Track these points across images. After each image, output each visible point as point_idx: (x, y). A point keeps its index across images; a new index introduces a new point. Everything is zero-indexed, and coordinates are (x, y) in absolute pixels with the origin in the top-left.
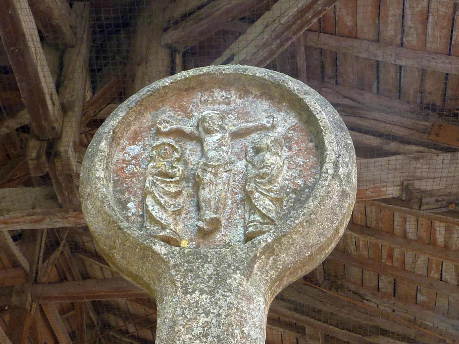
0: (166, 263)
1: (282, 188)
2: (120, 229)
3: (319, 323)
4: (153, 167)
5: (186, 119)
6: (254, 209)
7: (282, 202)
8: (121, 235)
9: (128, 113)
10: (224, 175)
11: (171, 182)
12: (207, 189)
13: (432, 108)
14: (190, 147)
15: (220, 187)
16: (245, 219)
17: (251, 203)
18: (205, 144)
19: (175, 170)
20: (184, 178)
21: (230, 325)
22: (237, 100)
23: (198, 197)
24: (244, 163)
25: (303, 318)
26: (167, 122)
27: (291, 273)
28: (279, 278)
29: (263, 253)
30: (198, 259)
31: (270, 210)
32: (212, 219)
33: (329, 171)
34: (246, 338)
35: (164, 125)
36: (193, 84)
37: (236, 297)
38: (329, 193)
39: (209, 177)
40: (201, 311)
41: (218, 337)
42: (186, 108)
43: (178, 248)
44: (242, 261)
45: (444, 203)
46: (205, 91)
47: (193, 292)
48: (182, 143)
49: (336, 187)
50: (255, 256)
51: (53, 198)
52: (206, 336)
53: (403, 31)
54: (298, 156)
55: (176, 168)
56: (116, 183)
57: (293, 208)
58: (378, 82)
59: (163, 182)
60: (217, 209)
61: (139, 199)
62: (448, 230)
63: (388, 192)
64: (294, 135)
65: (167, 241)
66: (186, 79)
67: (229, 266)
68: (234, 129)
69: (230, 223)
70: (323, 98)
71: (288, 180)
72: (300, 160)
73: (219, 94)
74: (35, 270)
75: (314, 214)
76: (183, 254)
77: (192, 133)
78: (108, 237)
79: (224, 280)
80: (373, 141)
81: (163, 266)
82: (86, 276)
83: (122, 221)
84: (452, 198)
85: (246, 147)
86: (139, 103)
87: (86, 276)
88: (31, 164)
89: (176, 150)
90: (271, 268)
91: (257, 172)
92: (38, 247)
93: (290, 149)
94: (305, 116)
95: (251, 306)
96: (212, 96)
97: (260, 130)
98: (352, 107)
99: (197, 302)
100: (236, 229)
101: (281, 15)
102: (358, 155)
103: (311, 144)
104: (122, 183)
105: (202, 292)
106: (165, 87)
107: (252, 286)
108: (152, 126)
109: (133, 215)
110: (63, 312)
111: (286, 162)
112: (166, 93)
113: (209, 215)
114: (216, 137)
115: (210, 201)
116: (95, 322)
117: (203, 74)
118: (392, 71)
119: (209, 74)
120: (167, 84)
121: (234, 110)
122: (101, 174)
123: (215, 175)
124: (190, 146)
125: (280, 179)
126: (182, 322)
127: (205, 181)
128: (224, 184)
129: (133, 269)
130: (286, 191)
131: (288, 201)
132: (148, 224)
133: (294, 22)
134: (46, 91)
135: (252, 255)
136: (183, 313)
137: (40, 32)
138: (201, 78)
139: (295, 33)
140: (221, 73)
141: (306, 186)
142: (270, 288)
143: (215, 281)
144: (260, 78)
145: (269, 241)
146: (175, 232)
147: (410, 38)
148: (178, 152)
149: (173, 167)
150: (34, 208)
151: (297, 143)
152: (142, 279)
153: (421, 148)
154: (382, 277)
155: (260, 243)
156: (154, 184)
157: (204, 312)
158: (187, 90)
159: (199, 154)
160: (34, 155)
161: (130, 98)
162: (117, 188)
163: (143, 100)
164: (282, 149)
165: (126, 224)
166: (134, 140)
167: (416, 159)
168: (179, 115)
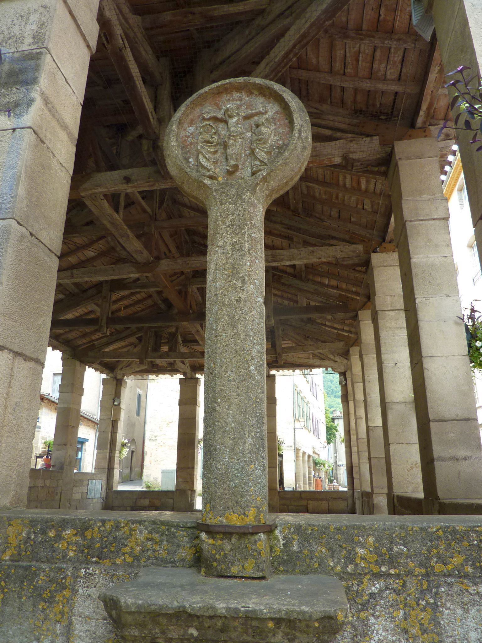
0: (210, 189)
1: (271, 146)
2: (186, 172)
3: (300, 235)
4: (202, 138)
5: (218, 110)
6: (256, 158)
7: (271, 154)
8: (187, 176)
9: (186, 108)
10: (240, 140)
11: (212, 146)
12: (231, 149)
13: (361, 111)
14: (221, 126)
15: (238, 147)
16: (251, 164)
17: (254, 155)
18: (229, 124)
19: (214, 139)
20: (218, 144)
21: (245, 219)
22: (246, 98)
23: (226, 154)
24: (250, 133)
25: (291, 232)
26: (208, 113)
27: (276, 192)
28: (270, 195)
29: (261, 181)
30: (227, 186)
31: (264, 158)
32: (234, 165)
33: (296, 135)
34: (253, 226)
35: (206, 114)
36: (221, 89)
37: (248, 206)
38: (296, 147)
39: (231, 142)
40: (230, 213)
41: (239, 226)
42: (218, 104)
43: (217, 181)
44: (250, 186)
46: (229, 93)
47: (225, 204)
48: (216, 124)
49: (300, 144)
50: (257, 183)
51: (159, 172)
52: (233, 226)
53: (345, 67)
54: (279, 128)
55: (214, 138)
56: (182, 148)
57: (277, 157)
59: (207, 146)
60: (237, 159)
61: (195, 157)
62: (368, 182)
63: (335, 161)
64: (278, 116)
65: (211, 177)
66: (217, 87)
67: (244, 189)
68: (244, 114)
69: (244, 167)
70: (293, 94)
71: (274, 142)
72: (280, 130)
73: (236, 95)
74: (154, 214)
75: (288, 159)
76: (219, 184)
77: (221, 118)
79: (241, 196)
80: (328, 132)
81: (209, 191)
82: (181, 216)
83: (187, 168)
85: (251, 125)
86: (192, 102)
87: (181, 216)
88: (145, 153)
89: (213, 128)
90: (266, 189)
91: (257, 138)
92: (155, 201)
93: (275, 124)
94: (283, 105)
95: (256, 210)
96: (232, 96)
97: (259, 114)
99: (227, 209)
100: (247, 170)
101: (276, 57)
102: (312, 125)
103: (287, 121)
104: (186, 148)
105: (230, 203)
106: (206, 92)
107: (256, 199)
108: (200, 116)
109: (193, 165)
110: (171, 236)
111: (273, 132)
112: (207, 96)
113: (232, 162)
114: (235, 119)
115: (232, 155)
116: (188, 240)
117: (226, 84)
118: (339, 91)
119: (230, 83)
120: (207, 90)
121: (244, 103)
122: (174, 143)
123: (235, 141)
124: (221, 125)
125: (269, 142)
126: (220, 219)
127: (230, 144)
128: (240, 145)
129: (195, 194)
130: (273, 148)
131: (274, 153)
132: (200, 170)
133: (283, 61)
134: (148, 110)
135: (255, 182)
136: (221, 215)
137: (143, 78)
138: (225, 86)
139: (283, 68)
140: (236, 82)
141: (284, 144)
142: (266, 200)
143: (236, 198)
144: (258, 84)
145: (264, 174)
146: (215, 173)
147: (348, 70)
148: (214, 129)
149: (212, 138)
150: (149, 178)
151: (279, 121)
153: (353, 135)
154: (333, 209)
155: (259, 176)
156: (202, 147)
157: (231, 214)
158: (218, 94)
159: (226, 129)
161: (187, 100)
162: (184, 151)
163: (194, 101)
164: (271, 124)
165: (189, 170)
166: (191, 124)
167: (351, 141)
168: (214, 108)
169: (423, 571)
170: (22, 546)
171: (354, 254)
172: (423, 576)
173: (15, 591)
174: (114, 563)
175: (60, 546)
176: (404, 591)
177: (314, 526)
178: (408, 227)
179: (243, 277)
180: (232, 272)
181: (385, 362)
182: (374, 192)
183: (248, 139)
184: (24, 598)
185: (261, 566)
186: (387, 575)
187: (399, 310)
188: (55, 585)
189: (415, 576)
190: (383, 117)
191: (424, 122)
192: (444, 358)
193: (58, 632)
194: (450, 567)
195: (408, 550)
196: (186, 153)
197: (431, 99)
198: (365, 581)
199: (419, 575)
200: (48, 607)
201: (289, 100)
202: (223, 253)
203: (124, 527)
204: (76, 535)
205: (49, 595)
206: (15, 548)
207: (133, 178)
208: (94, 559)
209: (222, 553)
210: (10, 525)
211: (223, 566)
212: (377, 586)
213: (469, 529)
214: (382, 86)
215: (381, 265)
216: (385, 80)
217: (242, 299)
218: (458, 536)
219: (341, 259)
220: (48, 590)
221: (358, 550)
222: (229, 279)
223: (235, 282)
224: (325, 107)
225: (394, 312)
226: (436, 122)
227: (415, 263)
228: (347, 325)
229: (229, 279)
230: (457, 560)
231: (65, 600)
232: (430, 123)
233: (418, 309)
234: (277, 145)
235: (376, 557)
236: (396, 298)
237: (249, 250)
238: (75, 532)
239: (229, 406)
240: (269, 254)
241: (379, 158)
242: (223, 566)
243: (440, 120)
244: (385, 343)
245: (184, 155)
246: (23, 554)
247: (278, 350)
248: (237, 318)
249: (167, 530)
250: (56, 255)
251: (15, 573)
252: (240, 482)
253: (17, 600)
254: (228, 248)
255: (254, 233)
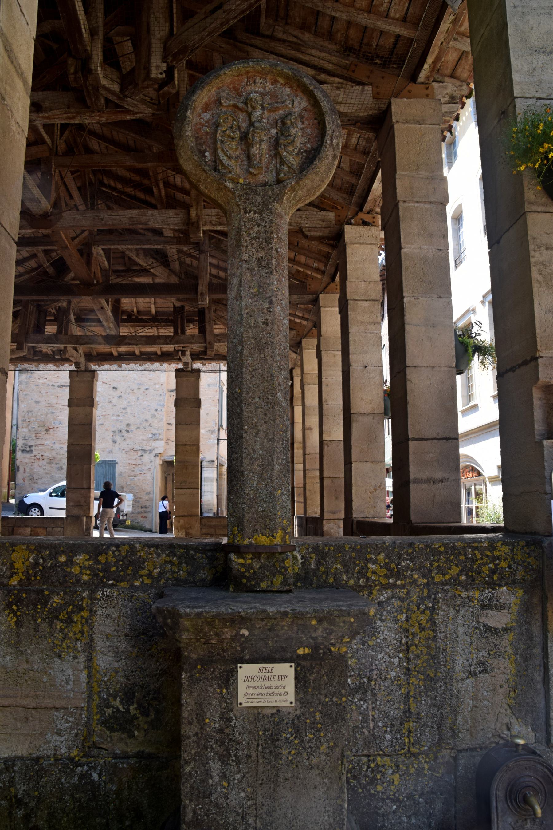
24: (275, 130)
41: (265, 239)
45: (354, 122)
58: (316, 27)
67: (270, 197)
78: (196, 175)
84: (359, 119)
90: (293, 199)
93: (303, 123)
94: (312, 101)
98: (296, 44)
103: (316, 121)
105: (255, 213)
150: (69, 107)
151: (307, 120)
152: (217, 201)
153: (341, 81)
160: (72, 71)
167: (338, 88)
169: (425, 581)
170: (31, 572)
171: (324, 224)
172: (424, 585)
173: (29, 614)
174: (132, 586)
175: (73, 570)
176: (407, 599)
177: (331, 546)
178: (401, 209)
179: (270, 297)
180: (259, 292)
181: (353, 364)
182: (355, 149)
183: (273, 137)
184: (40, 620)
185: (289, 581)
186: (394, 586)
187: (374, 300)
188: (71, 607)
189: (419, 586)
190: (378, 61)
191: (428, 78)
192: (429, 369)
193: (80, 649)
194: (447, 577)
195: (414, 565)
196: (201, 145)
197: (439, 52)
198: (375, 592)
199: (420, 585)
200: (66, 627)
201: (321, 99)
202: (248, 269)
203: (139, 551)
204: (88, 560)
205: (66, 616)
206: (23, 573)
207: (47, 104)
208: (110, 582)
209: (252, 571)
210: (14, 551)
211: (253, 583)
212: (385, 595)
213: (466, 545)
214: (382, 25)
215: (356, 241)
216: (387, 17)
217: (269, 321)
218: (456, 551)
219: (307, 229)
220: (65, 612)
221: (370, 566)
222: (256, 299)
223: (261, 302)
224: (307, 37)
225: (368, 302)
226: (440, 78)
227: (406, 253)
228: (301, 310)
229: (256, 299)
230: (455, 571)
231: (84, 620)
232: (434, 78)
233: (405, 310)
234: (305, 149)
235: (385, 571)
236: (372, 285)
237: (276, 268)
238: (87, 557)
239: (257, 433)
240: (214, 213)
241: (371, 115)
242: (253, 583)
243: (446, 76)
244: (355, 341)
245: (199, 147)
246: (33, 579)
247: (209, 338)
248: (264, 341)
249: (186, 553)
250: (13, 239)
251: (26, 597)
252: (268, 507)
253: (32, 622)
254: (254, 263)
255: (281, 248)
